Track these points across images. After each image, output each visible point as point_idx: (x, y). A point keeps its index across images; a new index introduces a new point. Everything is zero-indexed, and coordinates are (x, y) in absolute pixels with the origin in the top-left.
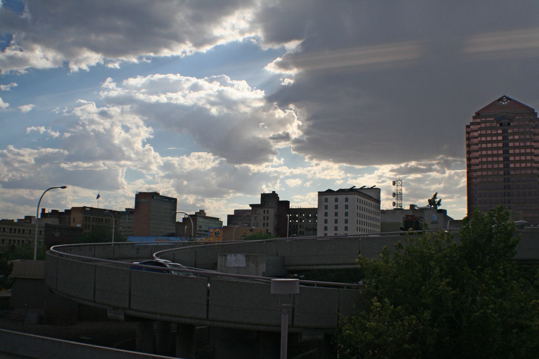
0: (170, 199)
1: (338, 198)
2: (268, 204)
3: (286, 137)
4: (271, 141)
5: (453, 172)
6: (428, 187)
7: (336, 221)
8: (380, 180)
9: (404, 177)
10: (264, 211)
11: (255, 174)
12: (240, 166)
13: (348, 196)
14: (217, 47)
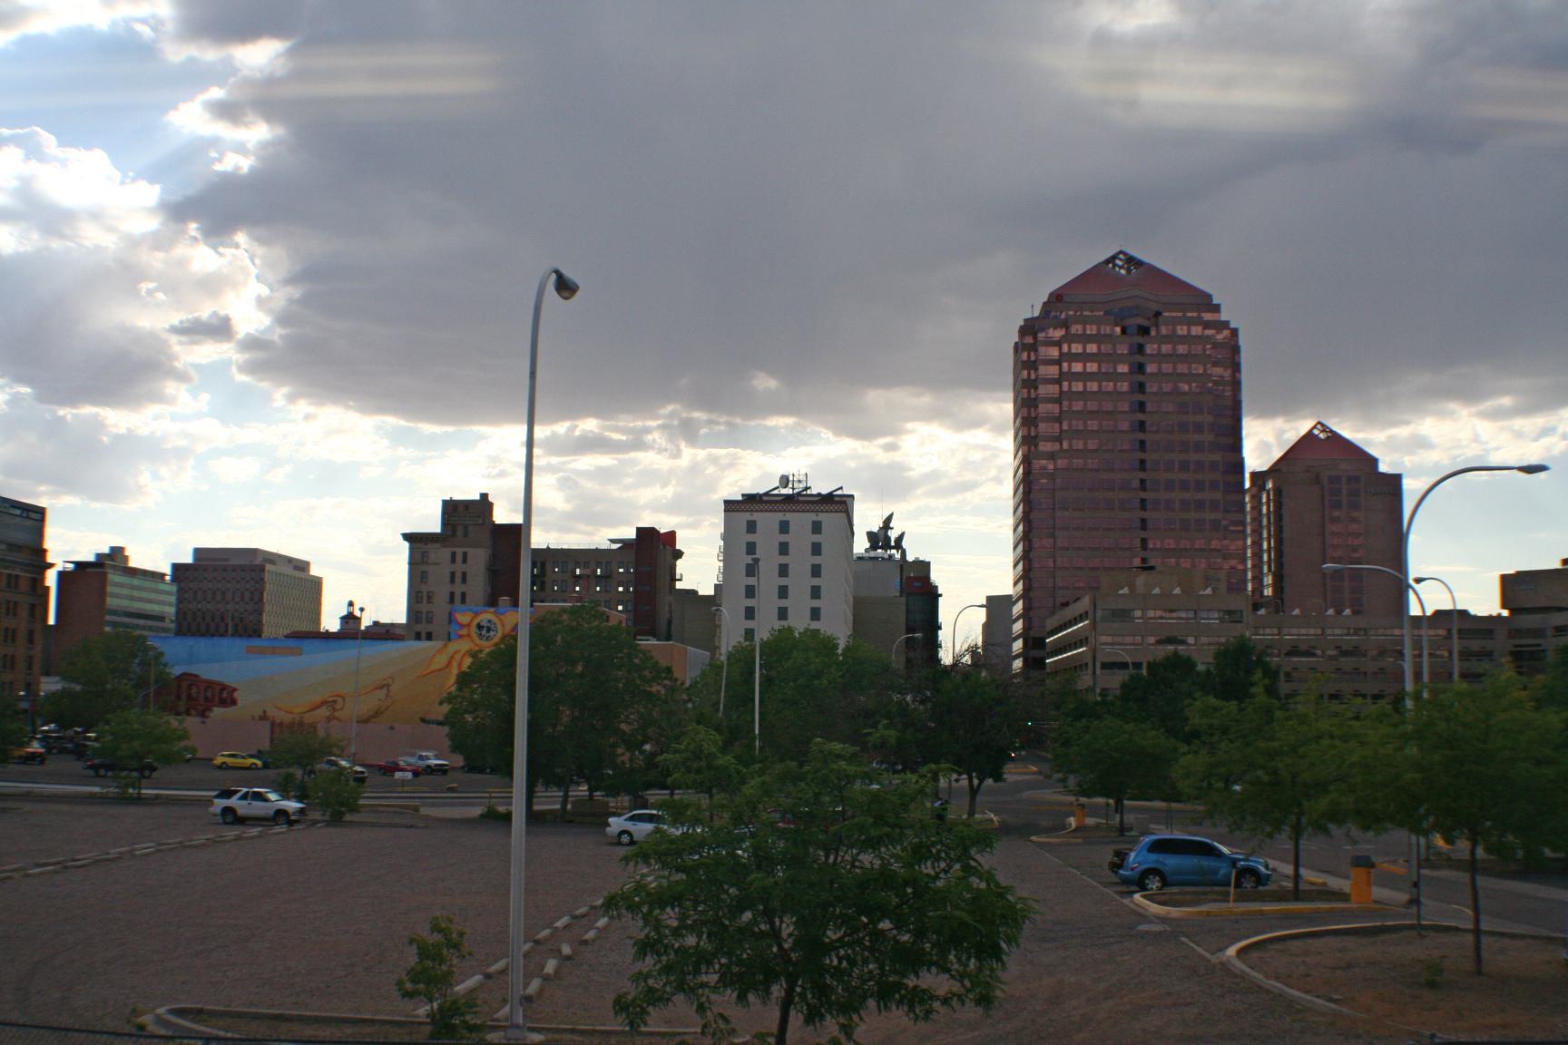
0: (28, 510)
1: (820, 522)
2: (466, 534)
3: (220, 329)
4: (174, 339)
5: (701, 454)
6: (631, 494)
7: (783, 592)
8: (493, 468)
9: (563, 463)
10: (454, 555)
11: (118, 439)
12: (75, 411)
13: (822, 517)
14: (25, 42)
